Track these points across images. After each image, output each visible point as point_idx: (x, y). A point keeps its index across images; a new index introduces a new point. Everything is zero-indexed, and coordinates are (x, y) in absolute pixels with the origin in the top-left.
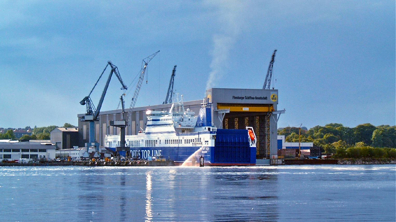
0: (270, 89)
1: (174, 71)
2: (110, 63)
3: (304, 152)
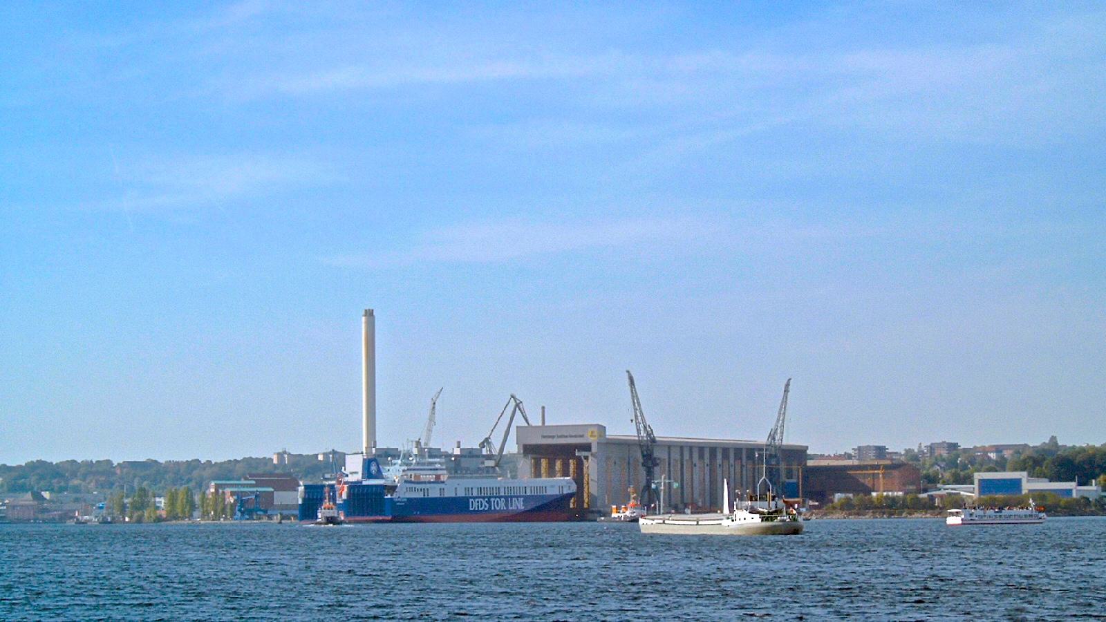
0: (546, 424)
1: (787, 385)
2: (513, 397)
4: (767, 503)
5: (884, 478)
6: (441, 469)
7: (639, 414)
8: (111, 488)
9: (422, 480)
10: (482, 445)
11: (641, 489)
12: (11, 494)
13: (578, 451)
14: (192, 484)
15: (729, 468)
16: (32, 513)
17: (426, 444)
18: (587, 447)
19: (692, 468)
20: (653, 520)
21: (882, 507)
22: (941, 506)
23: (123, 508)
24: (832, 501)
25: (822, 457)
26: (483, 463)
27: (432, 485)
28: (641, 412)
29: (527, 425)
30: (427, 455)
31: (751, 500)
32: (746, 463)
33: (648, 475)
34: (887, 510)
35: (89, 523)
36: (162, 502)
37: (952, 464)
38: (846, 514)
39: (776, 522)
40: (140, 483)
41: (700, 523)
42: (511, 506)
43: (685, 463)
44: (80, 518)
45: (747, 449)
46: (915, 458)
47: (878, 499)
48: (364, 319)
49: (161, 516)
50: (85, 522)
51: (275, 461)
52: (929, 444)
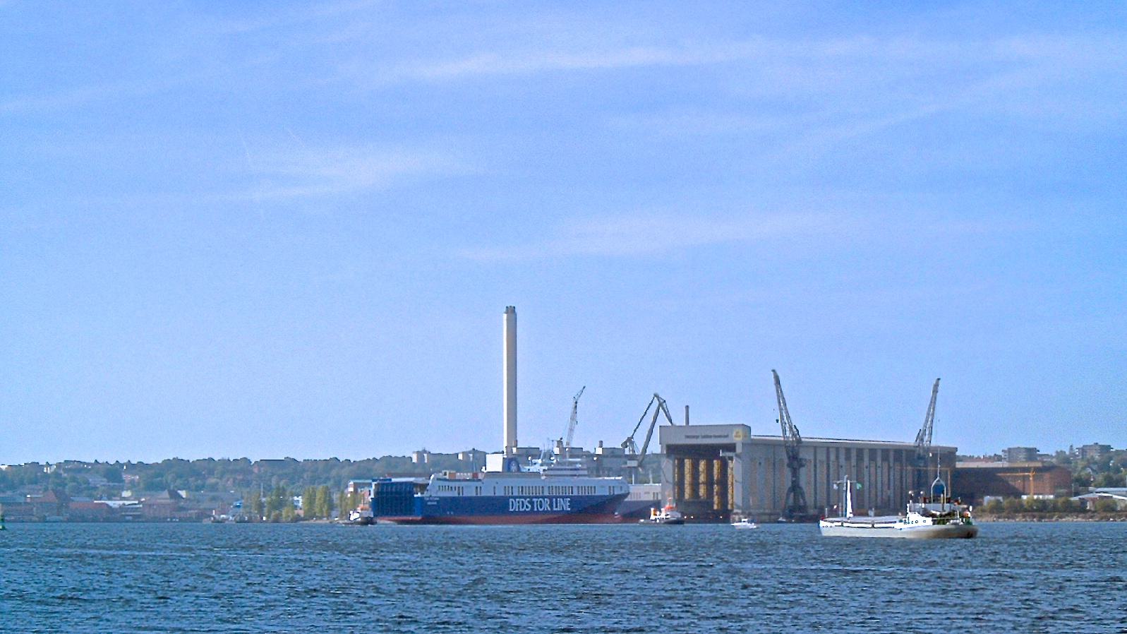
0: (690, 424)
1: (936, 386)
2: (656, 395)
3: (699, 489)
4: (941, 505)
5: (1034, 480)
6: (582, 469)
7: (784, 415)
8: (248, 486)
9: (457, 478)
10: (625, 445)
11: (786, 491)
12: (148, 492)
13: (722, 452)
14: (330, 484)
15: (876, 469)
16: (168, 511)
17: (568, 444)
18: (731, 448)
19: (838, 468)
20: (832, 522)
21: (1034, 511)
22: (1093, 509)
23: (261, 506)
24: (981, 504)
25: (971, 459)
26: (626, 463)
27: (466, 483)
28: (787, 412)
29: (670, 425)
30: (567, 455)
31: (925, 502)
32: (894, 464)
33: (793, 477)
34: (1036, 514)
35: (227, 522)
36: (300, 500)
37: (1104, 466)
38: (995, 517)
39: (948, 525)
40: (278, 483)
41: (875, 526)
42: (557, 507)
43: (831, 466)
44: (217, 517)
45: (906, 450)
46: (1067, 460)
47: (1028, 502)
48: (505, 316)
49: (298, 515)
50: (223, 521)
51: (415, 460)
52: (1081, 446)
